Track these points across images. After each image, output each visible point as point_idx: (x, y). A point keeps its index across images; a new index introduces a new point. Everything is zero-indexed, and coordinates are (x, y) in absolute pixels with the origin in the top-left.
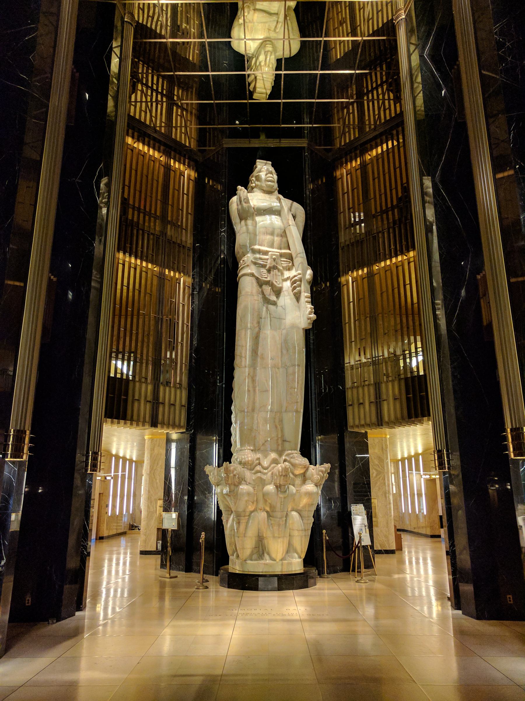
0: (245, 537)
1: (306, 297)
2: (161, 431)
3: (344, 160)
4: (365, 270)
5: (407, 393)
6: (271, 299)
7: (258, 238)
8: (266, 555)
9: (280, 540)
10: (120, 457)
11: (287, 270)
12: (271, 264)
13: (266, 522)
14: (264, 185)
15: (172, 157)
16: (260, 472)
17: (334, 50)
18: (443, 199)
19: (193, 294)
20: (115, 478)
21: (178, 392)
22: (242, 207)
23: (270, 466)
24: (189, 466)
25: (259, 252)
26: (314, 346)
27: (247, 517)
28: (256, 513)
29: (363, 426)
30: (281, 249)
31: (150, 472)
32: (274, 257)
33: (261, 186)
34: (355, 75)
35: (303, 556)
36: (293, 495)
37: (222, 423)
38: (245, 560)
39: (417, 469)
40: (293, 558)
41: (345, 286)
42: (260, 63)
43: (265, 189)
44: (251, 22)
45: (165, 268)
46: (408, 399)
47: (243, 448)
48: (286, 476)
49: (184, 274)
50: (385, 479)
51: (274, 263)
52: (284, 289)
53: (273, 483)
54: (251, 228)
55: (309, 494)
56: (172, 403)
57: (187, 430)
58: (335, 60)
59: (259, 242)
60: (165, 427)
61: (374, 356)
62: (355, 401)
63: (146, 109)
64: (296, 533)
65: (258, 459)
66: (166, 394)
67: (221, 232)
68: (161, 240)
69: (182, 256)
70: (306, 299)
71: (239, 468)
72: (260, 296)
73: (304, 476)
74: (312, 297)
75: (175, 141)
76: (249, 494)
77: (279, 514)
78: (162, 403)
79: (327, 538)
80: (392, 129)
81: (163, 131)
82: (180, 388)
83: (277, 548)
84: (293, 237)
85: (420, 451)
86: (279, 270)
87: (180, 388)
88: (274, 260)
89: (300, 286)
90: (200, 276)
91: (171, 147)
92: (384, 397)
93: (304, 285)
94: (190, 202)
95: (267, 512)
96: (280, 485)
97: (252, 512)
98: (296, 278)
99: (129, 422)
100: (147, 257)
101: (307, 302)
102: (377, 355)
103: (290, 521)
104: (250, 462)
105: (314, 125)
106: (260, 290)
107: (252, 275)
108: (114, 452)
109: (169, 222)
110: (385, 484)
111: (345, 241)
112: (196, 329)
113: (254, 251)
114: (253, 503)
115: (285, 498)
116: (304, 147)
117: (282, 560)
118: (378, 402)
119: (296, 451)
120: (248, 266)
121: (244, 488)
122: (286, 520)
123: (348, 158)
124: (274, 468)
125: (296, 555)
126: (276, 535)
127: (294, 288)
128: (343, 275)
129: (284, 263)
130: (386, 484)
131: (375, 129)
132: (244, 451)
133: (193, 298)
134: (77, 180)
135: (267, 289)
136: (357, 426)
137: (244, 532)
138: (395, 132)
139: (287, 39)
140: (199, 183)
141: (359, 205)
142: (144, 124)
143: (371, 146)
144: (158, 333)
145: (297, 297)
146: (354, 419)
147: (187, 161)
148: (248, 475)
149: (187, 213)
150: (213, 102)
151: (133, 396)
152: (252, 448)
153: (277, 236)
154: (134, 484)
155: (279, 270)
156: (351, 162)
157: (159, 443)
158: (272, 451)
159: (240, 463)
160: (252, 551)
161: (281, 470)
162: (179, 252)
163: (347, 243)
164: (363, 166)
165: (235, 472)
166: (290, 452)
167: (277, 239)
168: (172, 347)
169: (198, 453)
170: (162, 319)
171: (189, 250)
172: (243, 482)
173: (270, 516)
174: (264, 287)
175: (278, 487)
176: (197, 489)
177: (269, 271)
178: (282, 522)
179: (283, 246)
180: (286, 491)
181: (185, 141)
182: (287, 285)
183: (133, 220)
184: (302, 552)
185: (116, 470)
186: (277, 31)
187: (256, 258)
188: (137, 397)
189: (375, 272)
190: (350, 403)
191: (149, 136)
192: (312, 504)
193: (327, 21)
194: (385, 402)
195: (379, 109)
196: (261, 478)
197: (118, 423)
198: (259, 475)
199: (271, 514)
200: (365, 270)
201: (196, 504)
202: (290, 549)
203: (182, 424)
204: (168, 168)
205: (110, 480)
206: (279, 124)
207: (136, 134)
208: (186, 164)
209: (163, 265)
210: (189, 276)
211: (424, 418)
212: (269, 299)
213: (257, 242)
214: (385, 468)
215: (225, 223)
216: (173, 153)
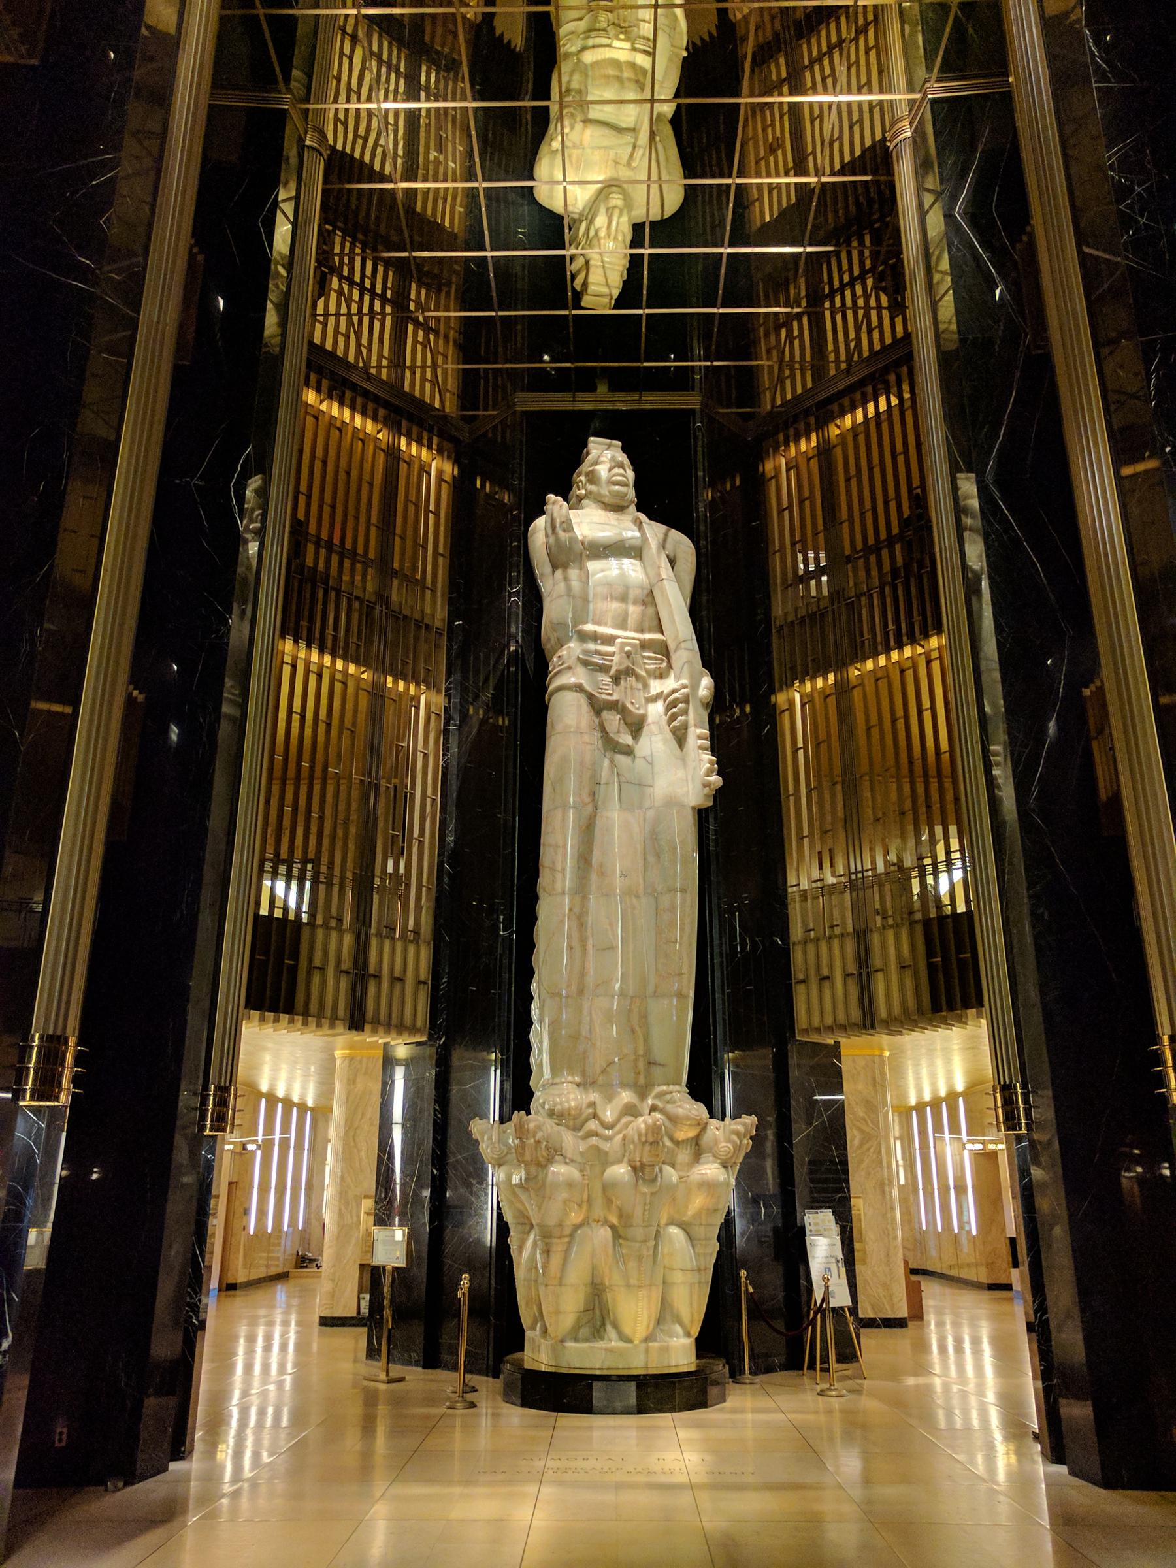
0: (560, 1285)
1: (700, 737)
2: (372, 1040)
3: (781, 437)
4: (831, 677)
5: (930, 954)
6: (621, 741)
7: (591, 606)
8: (609, 1327)
9: (642, 1293)
10: (279, 1100)
11: (655, 678)
12: (620, 663)
13: (610, 1251)
14: (604, 491)
15: (404, 430)
16: (596, 1134)
17: (757, 204)
18: (1004, 520)
19: (446, 732)
20: (267, 1146)
21: (412, 949)
22: (557, 539)
23: (618, 1120)
25: (595, 637)
26: (717, 846)
27: (566, 1240)
28: (586, 1229)
29: (830, 1029)
30: (642, 631)
31: (346, 1133)
32: (627, 648)
33: (600, 494)
35: (695, 1331)
36: (672, 1188)
37: (509, 1022)
38: (562, 1341)
39: (955, 1129)
40: (671, 1336)
41: (787, 714)
42: (596, 233)
43: (606, 500)
44: (579, 146)
46: (931, 968)
47: (557, 1080)
48: (655, 1143)
50: (880, 1152)
51: (627, 663)
52: (650, 720)
53: (626, 1159)
54: (575, 584)
55: (708, 1186)
56: (397, 974)
57: (430, 1037)
58: (758, 224)
59: (594, 615)
60: (381, 1029)
62: (812, 972)
63: (348, 329)
64: (678, 1277)
65: (593, 1104)
66: (384, 956)
68: (377, 612)
69: (423, 647)
70: (700, 742)
71: (550, 1125)
72: (597, 735)
73: (697, 1144)
74: (712, 737)
75: (410, 397)
76: (570, 1185)
77: (639, 1233)
78: (375, 976)
79: (751, 1289)
80: (886, 370)
83: (634, 1311)
84: (670, 605)
85: (960, 1087)
86: (638, 677)
87: (416, 941)
88: (628, 655)
89: (685, 712)
90: (464, 690)
91: (402, 412)
92: (877, 962)
93: (696, 710)
94: (442, 528)
95: (612, 1227)
96: (643, 1166)
97: (577, 1227)
98: (676, 695)
101: (700, 748)
102: (859, 869)
103: (664, 1249)
104: (573, 1112)
105: (716, 363)
106: (597, 721)
107: (579, 688)
108: (264, 1088)
109: (395, 573)
111: (786, 614)
112: (452, 808)
113: (583, 637)
114: (580, 1206)
115: (652, 1194)
116: (693, 411)
117: (647, 1339)
119: (677, 1088)
120: (569, 668)
121: (559, 1170)
122: (656, 1246)
123: (791, 432)
124: (627, 1125)
125: (678, 1329)
126: (633, 1281)
127: (673, 718)
128: (781, 689)
129: (649, 662)
132: (560, 1086)
133: (446, 741)
135: (612, 720)
136: (818, 1030)
137: (558, 1275)
138: (892, 378)
139: (655, 182)
140: (462, 489)
142: (343, 361)
145: (680, 737)
147: (435, 440)
148: (569, 1141)
150: (493, 314)
151: (310, 960)
152: (577, 1079)
153: (635, 603)
155: (638, 677)
157: (367, 1068)
158: (624, 1085)
159: (551, 1113)
160: (578, 1320)
161: (643, 1131)
162: (417, 639)
164: (825, 452)
165: (539, 1135)
166: (665, 1088)
167: (634, 611)
169: (454, 1089)
170: (377, 786)
172: (557, 1158)
173: (620, 1237)
174: (605, 714)
175: (638, 1169)
176: (451, 1173)
177: (616, 680)
178: (647, 1252)
179: (646, 625)
180: (654, 1180)
182: (656, 710)
184: (692, 1322)
185: (269, 1130)
186: (634, 164)
187: (587, 652)
188: (317, 962)
189: (854, 682)
190: (801, 976)
191: (354, 387)
192: (716, 1210)
194: (880, 976)
196: (597, 1149)
198: (594, 1140)
199: (621, 1231)
200: (831, 677)
202: (665, 1314)
203: (419, 1024)
204: (393, 456)
205: (254, 1152)
207: (325, 383)
209: (382, 669)
210: (439, 691)
211: (969, 1011)
212: (618, 742)
213: (590, 618)
214: (882, 1125)
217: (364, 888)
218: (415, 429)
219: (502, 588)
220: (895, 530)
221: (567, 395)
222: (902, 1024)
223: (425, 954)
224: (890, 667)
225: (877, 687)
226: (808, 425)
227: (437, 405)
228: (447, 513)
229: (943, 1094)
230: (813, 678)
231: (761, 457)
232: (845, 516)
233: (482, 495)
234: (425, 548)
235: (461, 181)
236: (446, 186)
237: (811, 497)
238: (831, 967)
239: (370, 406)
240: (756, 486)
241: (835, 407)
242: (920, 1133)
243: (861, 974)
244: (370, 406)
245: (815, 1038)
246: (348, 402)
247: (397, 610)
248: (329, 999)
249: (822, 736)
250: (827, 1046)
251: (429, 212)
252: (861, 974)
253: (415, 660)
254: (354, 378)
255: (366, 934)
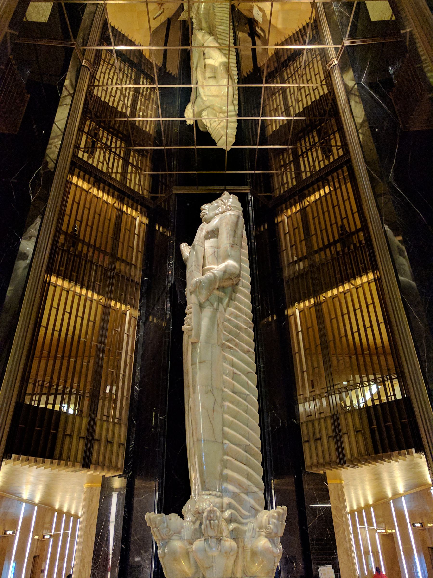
2: (95, 474)
3: (284, 206)
4: (312, 301)
5: (370, 423)
10: (64, 513)
15: (125, 202)
17: (270, 126)
18: (401, 196)
19: (138, 325)
20: (56, 537)
21: (117, 427)
24: (124, 517)
26: (264, 374)
29: (323, 465)
31: (86, 527)
34: (293, 122)
37: (163, 463)
39: (370, 523)
41: (292, 317)
45: (111, 298)
46: (372, 431)
49: (131, 307)
50: (344, 533)
56: (109, 440)
57: (125, 472)
58: (271, 133)
60: (99, 468)
61: (328, 385)
62: (312, 436)
63: (103, 161)
67: (169, 264)
68: (109, 273)
69: (130, 289)
75: (129, 188)
78: (98, 440)
80: (327, 175)
81: (118, 179)
82: (119, 424)
85: (371, 502)
90: (148, 307)
92: (344, 430)
94: (141, 242)
99: (57, 461)
100: (93, 287)
102: (332, 385)
105: (256, 172)
108: (57, 507)
109: (118, 259)
110: (345, 539)
111: (289, 275)
112: (139, 359)
118: (338, 436)
123: (288, 203)
128: (289, 307)
130: (347, 539)
131: (312, 176)
133: (138, 329)
134: (12, 180)
136: (316, 466)
138: (330, 178)
139: (230, 86)
140: (150, 228)
141: (301, 241)
142: (101, 171)
143: (309, 191)
144: (98, 363)
146: (311, 457)
147: (139, 207)
149: (138, 251)
150: (163, 148)
151: (65, 431)
154: (364, 568)
156: (291, 207)
162: (127, 285)
163: (291, 277)
164: (303, 210)
168: (115, 382)
169: (135, 500)
170: (104, 348)
171: (137, 284)
176: (132, 547)
181: (139, 189)
183: (81, 252)
185: (58, 529)
188: (68, 432)
189: (322, 301)
190: (306, 439)
191: (105, 182)
193: (263, 107)
194: (346, 437)
195: (314, 162)
197: (43, 462)
200: (312, 301)
201: (132, 567)
203: (119, 466)
205: (48, 540)
206: (224, 171)
207: (92, 179)
208: (139, 210)
209: (109, 297)
210: (136, 309)
211: (394, 453)
214: (344, 519)
215: (173, 258)
216: (126, 199)
217: (95, 397)
218: (130, 202)
219: (166, 262)
220: (337, 238)
221: (194, 188)
222: (359, 462)
223: (124, 430)
224: (339, 294)
225: (333, 302)
226: (295, 200)
227: (141, 192)
228: (143, 238)
229: (363, 505)
230: (304, 301)
231: (276, 215)
232: (313, 232)
233: (159, 233)
234: (133, 248)
235: (154, 118)
236: (149, 118)
237: (298, 227)
238: (320, 433)
239: (111, 190)
240: (274, 228)
241: (306, 192)
242: (353, 525)
243: (336, 436)
244: (111, 190)
245: (315, 470)
246: (101, 188)
247: (118, 272)
248: (73, 452)
249: (309, 325)
250: (320, 475)
251: (141, 125)
252: (336, 436)
253: (125, 294)
254: (105, 178)
255: (94, 419)
